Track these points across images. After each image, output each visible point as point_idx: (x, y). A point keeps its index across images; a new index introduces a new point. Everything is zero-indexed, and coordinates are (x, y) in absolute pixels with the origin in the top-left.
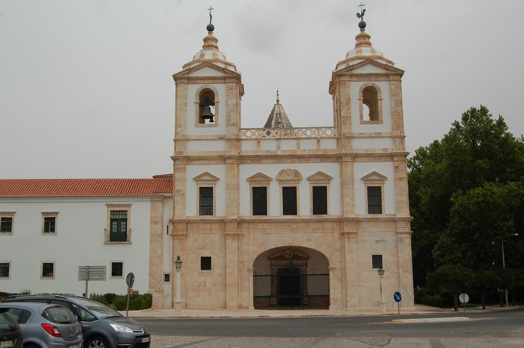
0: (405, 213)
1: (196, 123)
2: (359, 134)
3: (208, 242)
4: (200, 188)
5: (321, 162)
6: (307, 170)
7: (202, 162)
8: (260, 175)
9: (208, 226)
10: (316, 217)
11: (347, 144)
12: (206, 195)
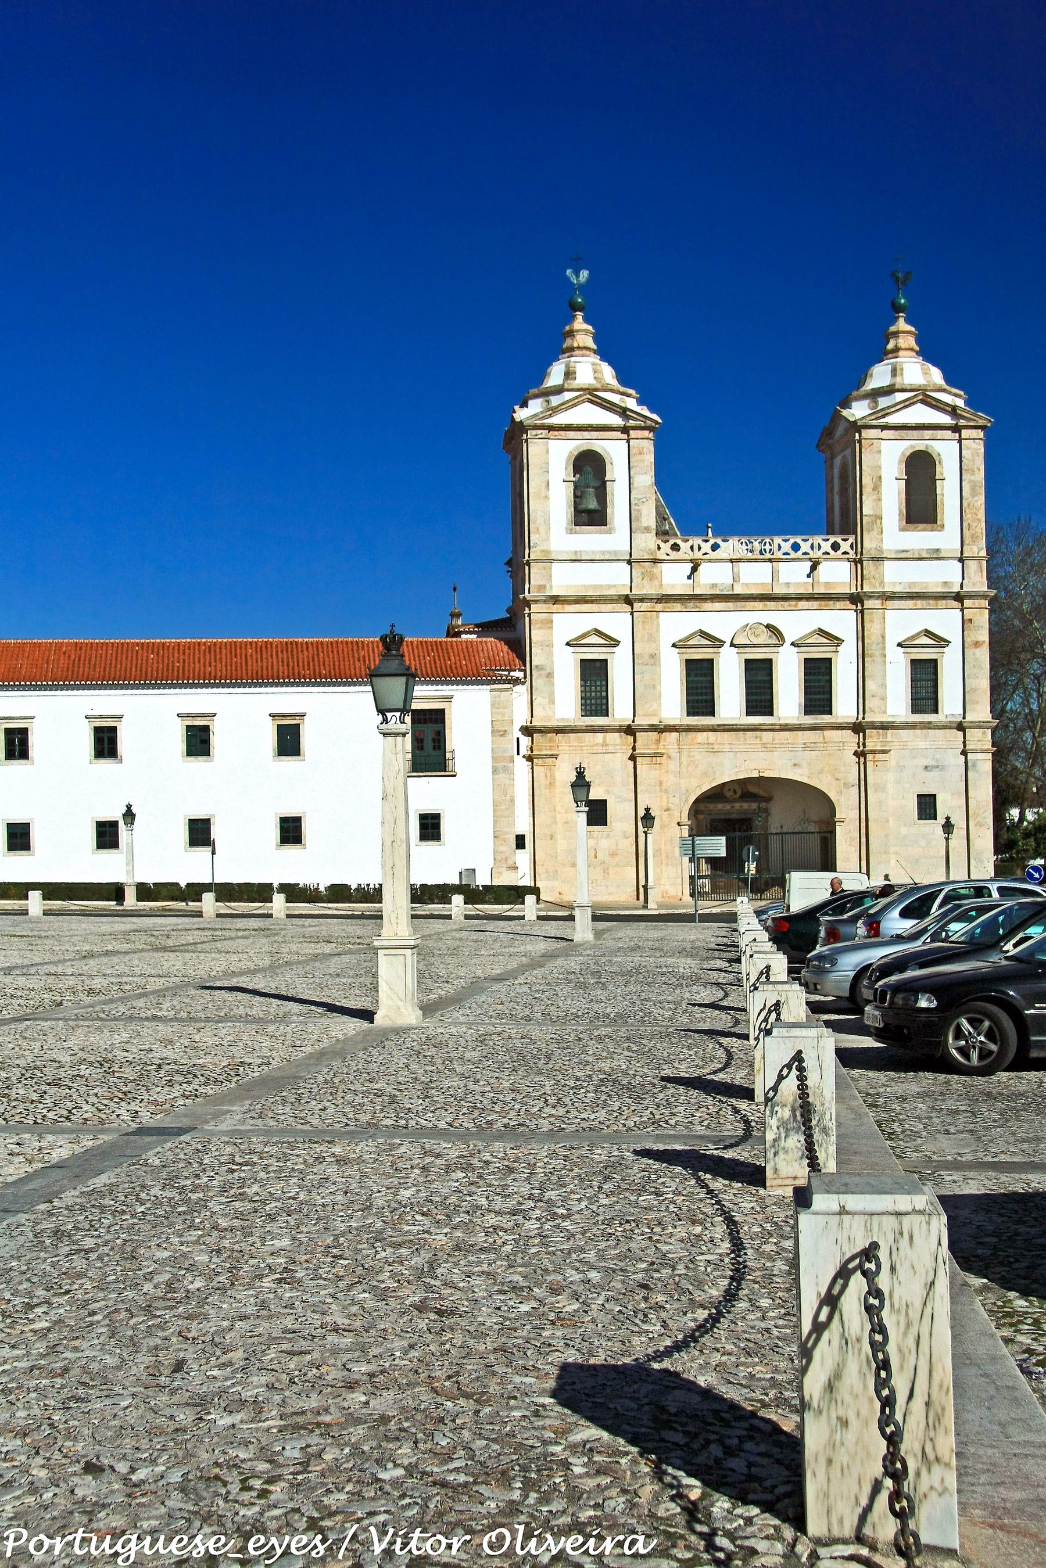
0: (982, 711)
1: (568, 524)
2: (897, 552)
4: (582, 660)
6: (797, 623)
10: (810, 720)
11: (873, 573)
12: (594, 675)
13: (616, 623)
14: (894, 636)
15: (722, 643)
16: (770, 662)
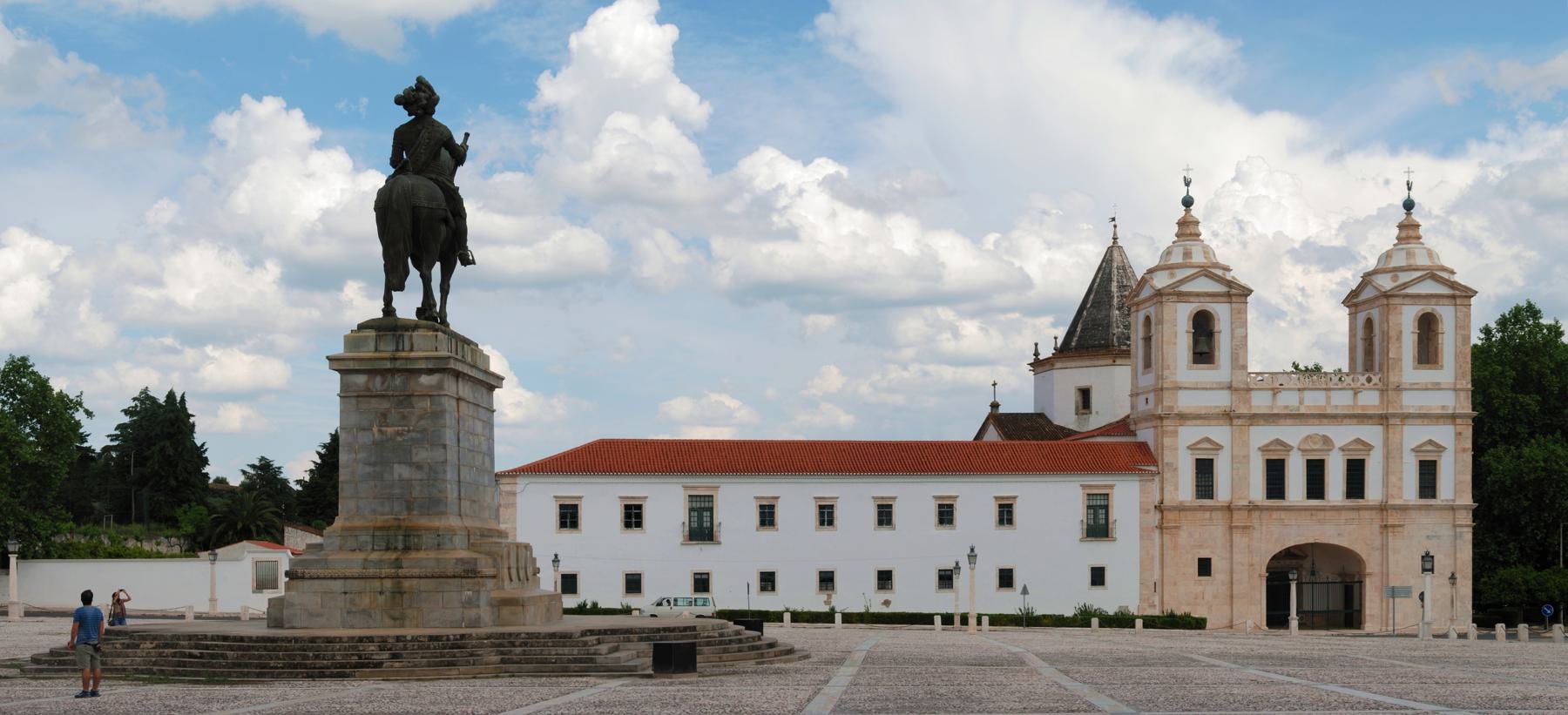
0: (1467, 499)
3: (1203, 535)
6: (1342, 435)
8: (1278, 442)
9: (1207, 515)
12: (1204, 469)
13: (1220, 433)
15: (1291, 448)
16: (1322, 461)
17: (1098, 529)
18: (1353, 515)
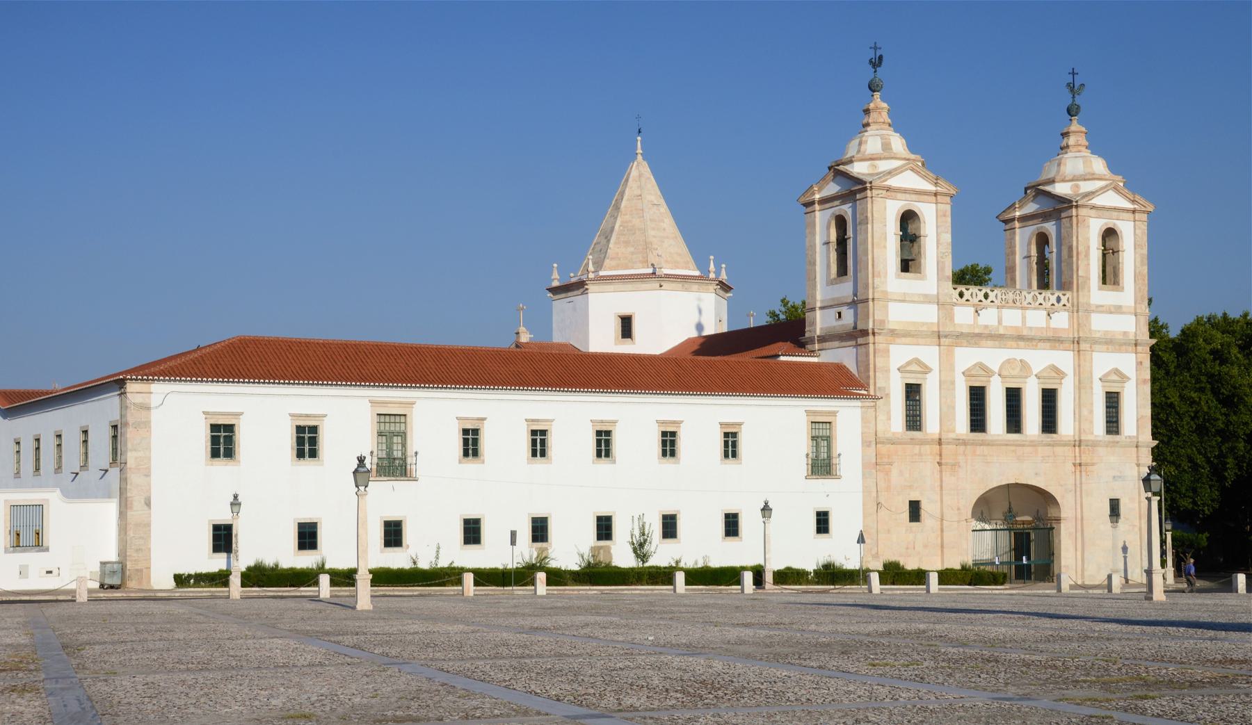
5: (1053, 348)
6: (1040, 359)
7: (908, 340)
12: (913, 392)
13: (929, 354)
14: (1098, 373)
17: (822, 466)
18: (1048, 450)
